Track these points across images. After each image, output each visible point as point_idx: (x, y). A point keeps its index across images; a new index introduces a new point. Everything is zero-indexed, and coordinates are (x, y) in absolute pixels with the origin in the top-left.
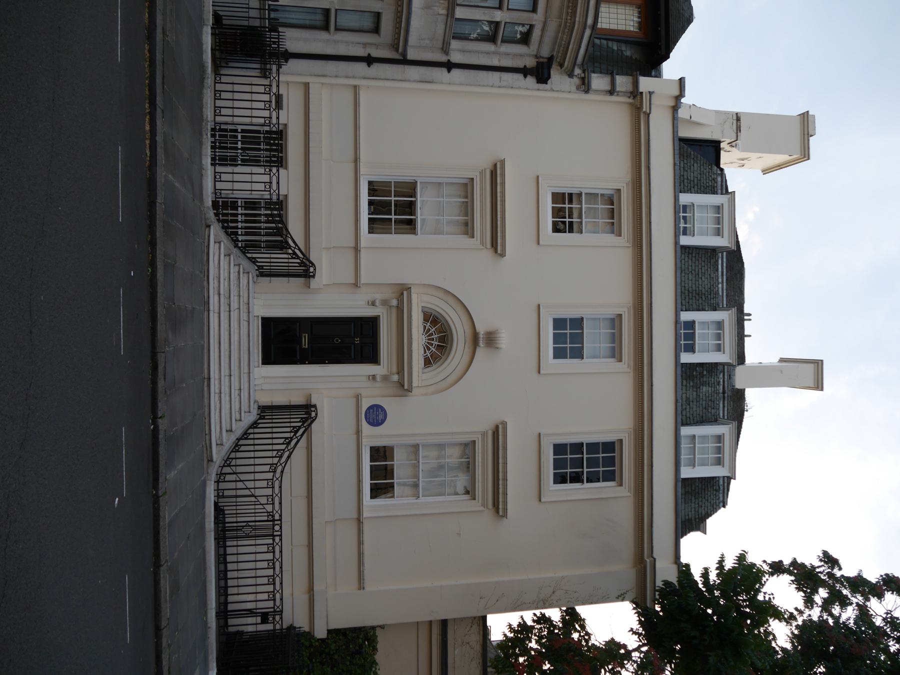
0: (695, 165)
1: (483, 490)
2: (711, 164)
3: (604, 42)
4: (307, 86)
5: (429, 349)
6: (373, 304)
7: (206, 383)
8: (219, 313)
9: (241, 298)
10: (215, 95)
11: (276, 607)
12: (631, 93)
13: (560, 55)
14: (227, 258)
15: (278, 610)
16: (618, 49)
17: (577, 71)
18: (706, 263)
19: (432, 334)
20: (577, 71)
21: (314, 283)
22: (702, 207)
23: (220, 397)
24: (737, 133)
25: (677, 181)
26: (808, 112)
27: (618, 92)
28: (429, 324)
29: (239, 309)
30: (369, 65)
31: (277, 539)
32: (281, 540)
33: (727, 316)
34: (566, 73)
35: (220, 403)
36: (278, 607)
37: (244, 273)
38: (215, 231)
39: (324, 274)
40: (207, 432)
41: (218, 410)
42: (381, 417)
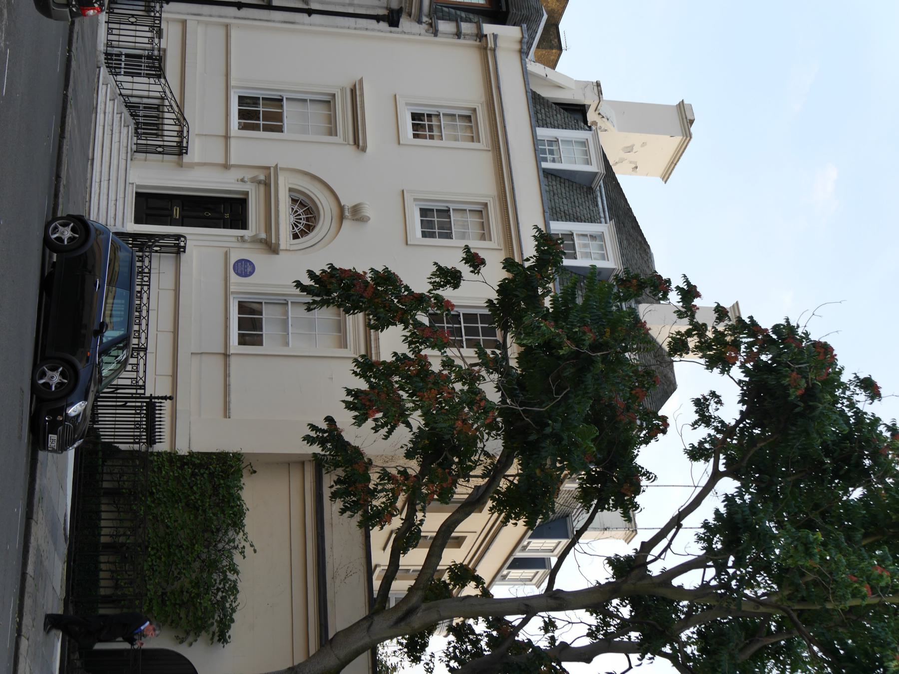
0: (558, 115)
1: (355, 340)
2: (577, 121)
3: (453, 11)
4: (184, 23)
5: (297, 226)
6: (242, 180)
7: (90, 163)
8: (104, 126)
9: (122, 134)
10: (108, 31)
11: (141, 345)
12: (477, 35)
13: (407, 5)
14: (112, 102)
15: (143, 347)
16: (466, 17)
17: (425, 19)
18: (582, 196)
19: (299, 215)
20: (425, 19)
21: (186, 159)
22: (568, 142)
23: (100, 184)
24: (599, 95)
25: (530, 101)
26: (683, 101)
27: (465, 35)
28: (296, 206)
29: (120, 142)
30: (239, 9)
31: (146, 288)
32: (149, 289)
33: (606, 229)
34: (415, 21)
35: (100, 189)
36: (143, 345)
37: (124, 126)
38: (104, 71)
39: (196, 151)
40: (87, 200)
41: (97, 195)
42: (249, 270)
